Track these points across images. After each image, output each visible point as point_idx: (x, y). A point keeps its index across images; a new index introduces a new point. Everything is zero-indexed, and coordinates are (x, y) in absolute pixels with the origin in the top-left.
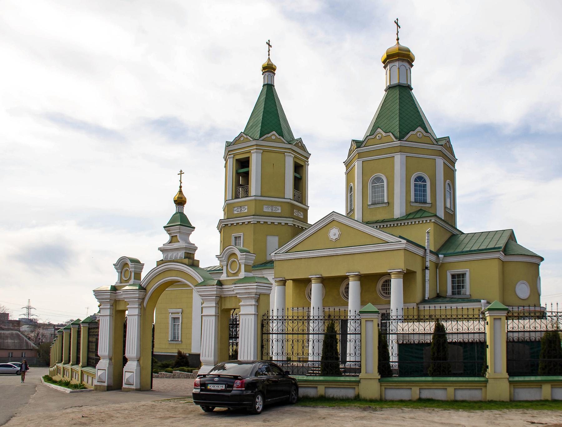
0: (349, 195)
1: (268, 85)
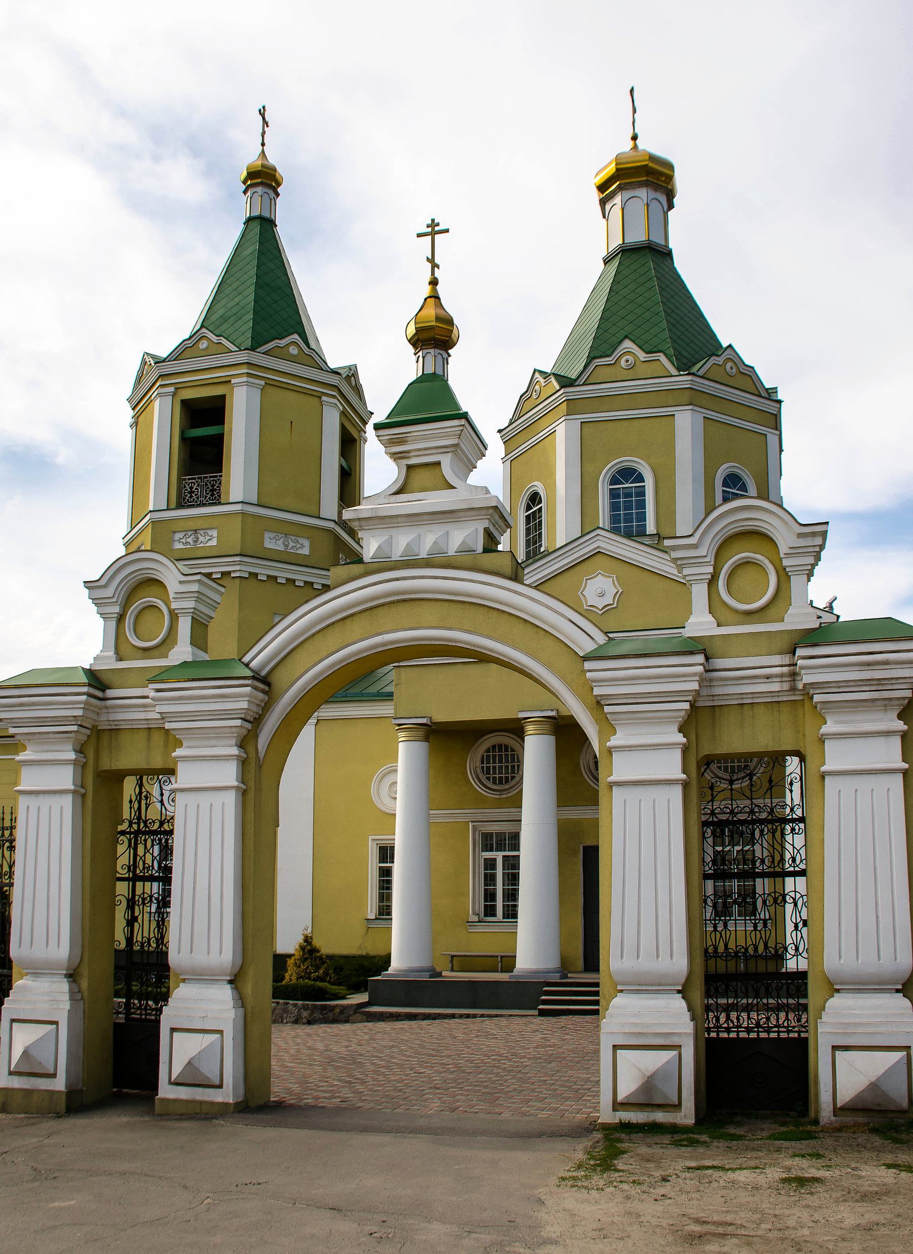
1: (260, 218)
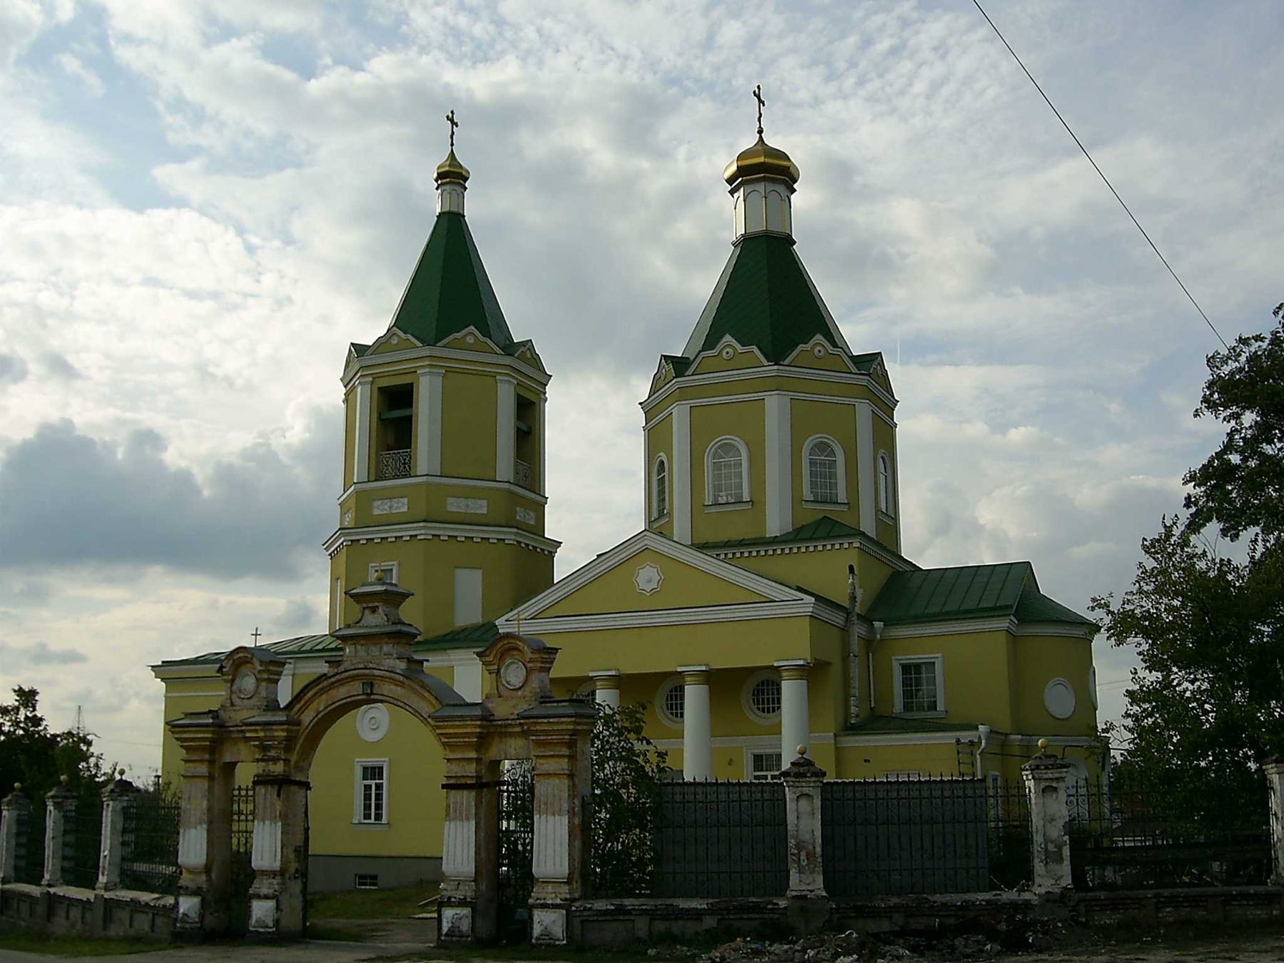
0: (655, 478)
1: (449, 213)
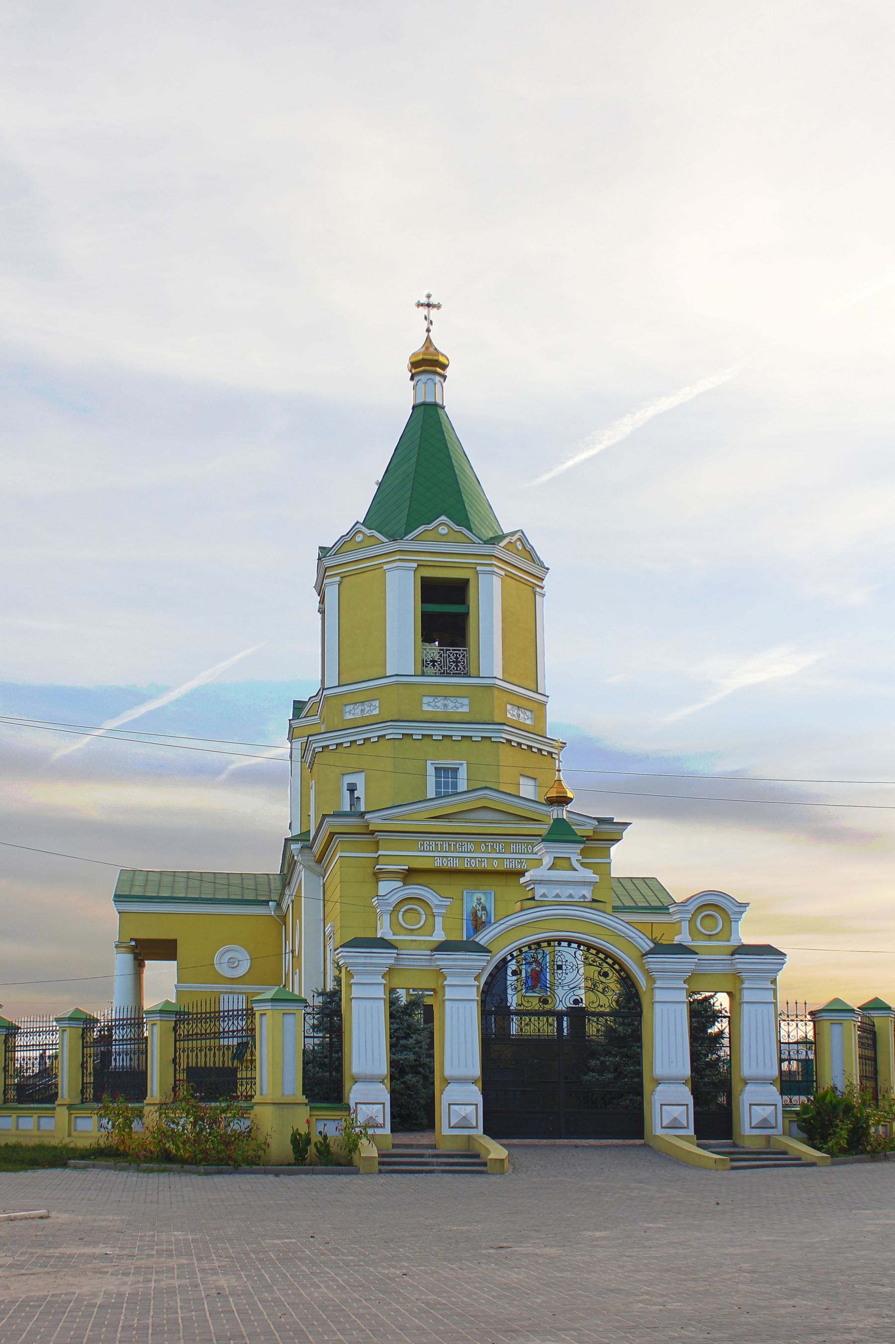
1: (424, 404)
